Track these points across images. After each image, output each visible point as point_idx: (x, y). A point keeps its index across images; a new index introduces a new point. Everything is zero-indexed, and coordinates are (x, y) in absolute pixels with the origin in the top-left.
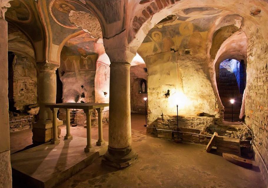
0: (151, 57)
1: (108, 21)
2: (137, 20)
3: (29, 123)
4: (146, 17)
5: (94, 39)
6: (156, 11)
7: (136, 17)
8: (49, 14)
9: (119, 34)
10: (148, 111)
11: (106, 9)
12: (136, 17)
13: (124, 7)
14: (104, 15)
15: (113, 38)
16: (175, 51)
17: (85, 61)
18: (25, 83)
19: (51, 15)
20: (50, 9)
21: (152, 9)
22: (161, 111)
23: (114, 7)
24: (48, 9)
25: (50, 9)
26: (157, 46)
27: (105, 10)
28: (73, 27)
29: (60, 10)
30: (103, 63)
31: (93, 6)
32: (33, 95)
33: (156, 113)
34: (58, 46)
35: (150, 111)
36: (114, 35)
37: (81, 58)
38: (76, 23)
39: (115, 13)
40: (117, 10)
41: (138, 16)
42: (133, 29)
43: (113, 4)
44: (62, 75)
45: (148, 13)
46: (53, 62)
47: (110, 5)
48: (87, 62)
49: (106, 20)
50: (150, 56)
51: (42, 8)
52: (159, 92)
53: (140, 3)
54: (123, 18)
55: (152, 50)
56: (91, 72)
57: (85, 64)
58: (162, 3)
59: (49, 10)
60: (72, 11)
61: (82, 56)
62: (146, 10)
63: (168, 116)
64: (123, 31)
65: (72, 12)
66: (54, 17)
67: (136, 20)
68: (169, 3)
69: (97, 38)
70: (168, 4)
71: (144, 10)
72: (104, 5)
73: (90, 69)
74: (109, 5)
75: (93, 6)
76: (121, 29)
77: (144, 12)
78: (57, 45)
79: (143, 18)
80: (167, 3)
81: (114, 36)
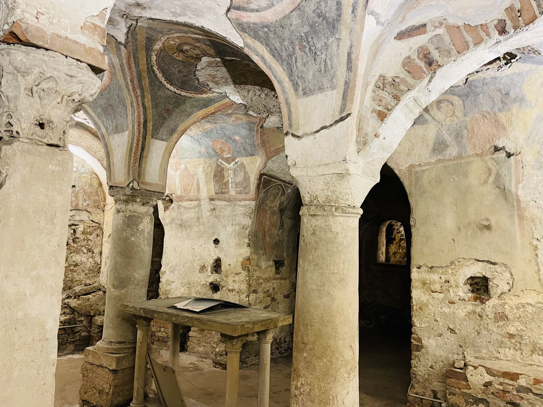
0: (424, 171)
1: (300, 88)
2: (384, 86)
3: (71, 336)
4: (414, 78)
5: (255, 117)
6: (446, 59)
7: (382, 77)
8: (150, 69)
9: (331, 125)
10: (412, 341)
11: (296, 58)
12: (382, 77)
13: (349, 55)
14: (290, 75)
15: (312, 137)
16: (509, 155)
17: (230, 172)
18: (73, 227)
19: (154, 71)
20: (154, 58)
21: (435, 55)
22: (461, 346)
23: (318, 53)
24: (148, 57)
25: (154, 58)
26: (448, 138)
27: (294, 61)
28: (206, 93)
29: (178, 58)
30: (275, 178)
31: (261, 51)
32: (90, 260)
33: (440, 352)
34: (165, 143)
35: (420, 340)
36: (315, 130)
37: (220, 164)
38: (212, 81)
39: (323, 68)
40: (328, 61)
41: (390, 75)
42: (373, 111)
43: (319, 46)
44: (166, 208)
45: (422, 64)
46: (150, 184)
47: (310, 49)
48: (232, 176)
49: (296, 86)
50: (420, 165)
51: (134, 57)
52: (452, 282)
53: (395, 38)
54: (346, 82)
55: (431, 148)
56: (243, 203)
57: (228, 181)
58: (465, 33)
59: (151, 61)
60: (205, 59)
61: (220, 160)
62: (415, 56)
63: (484, 370)
64: (342, 119)
65: (205, 60)
66: (160, 75)
67: (383, 84)
68: (488, 35)
69: (265, 115)
70: (485, 37)
71: (409, 57)
72: (291, 50)
73: (239, 196)
74: (307, 49)
75: (263, 51)
76: (337, 113)
77: (407, 63)
78: (162, 140)
79: (404, 81)
80: (483, 34)
81: (317, 132)
